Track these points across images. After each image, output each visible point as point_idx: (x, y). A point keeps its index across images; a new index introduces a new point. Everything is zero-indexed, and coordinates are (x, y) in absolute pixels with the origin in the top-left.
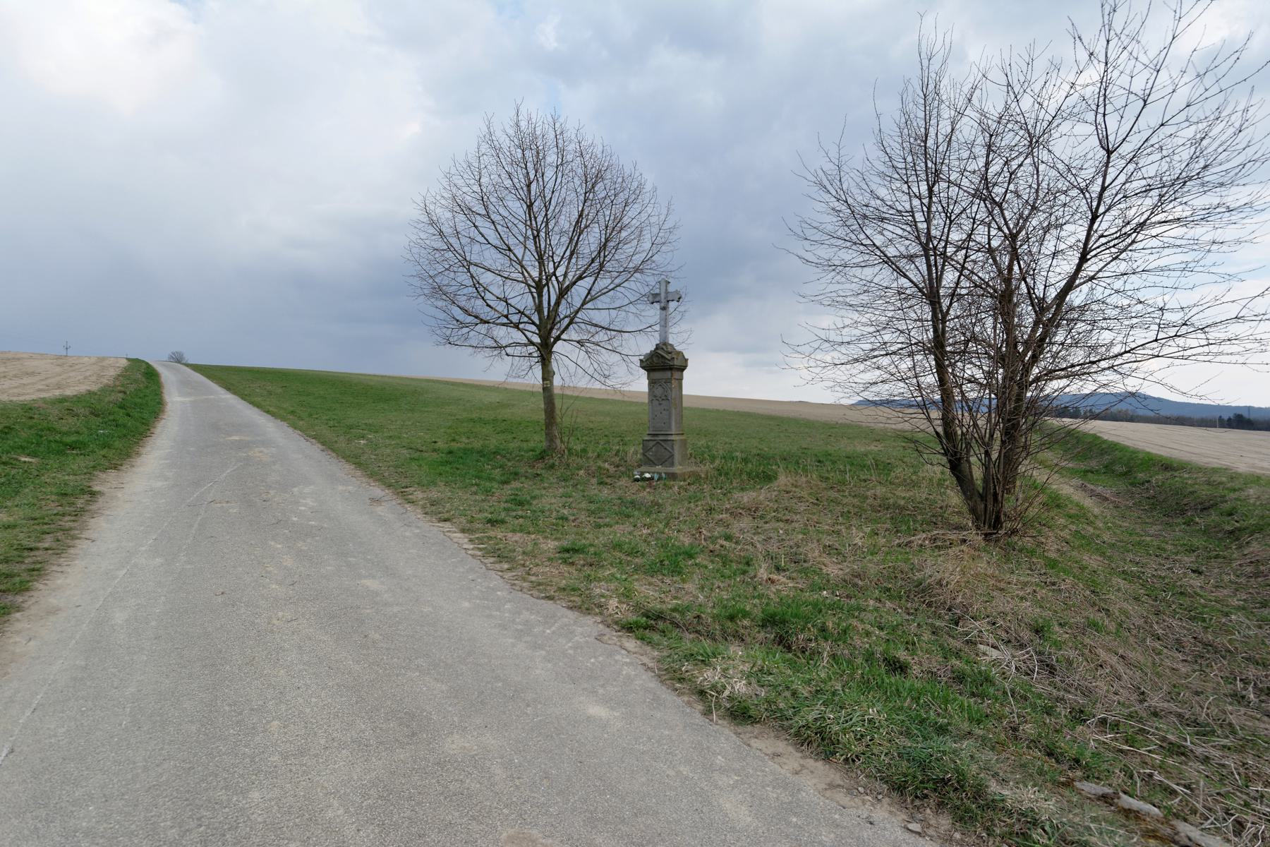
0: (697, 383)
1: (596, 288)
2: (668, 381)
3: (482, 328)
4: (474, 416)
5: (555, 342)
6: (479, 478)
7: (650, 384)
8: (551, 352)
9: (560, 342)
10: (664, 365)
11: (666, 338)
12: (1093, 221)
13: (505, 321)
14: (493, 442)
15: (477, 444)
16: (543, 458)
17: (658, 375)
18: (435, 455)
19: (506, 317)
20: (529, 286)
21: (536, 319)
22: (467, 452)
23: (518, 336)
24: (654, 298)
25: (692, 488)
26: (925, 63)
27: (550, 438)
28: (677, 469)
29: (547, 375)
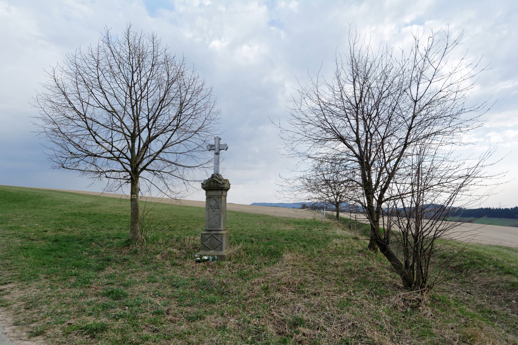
0: (236, 197)
1: (173, 139)
2: (220, 197)
3: (90, 159)
4: (76, 211)
5: (142, 170)
6: (77, 266)
7: (207, 198)
8: (138, 177)
9: (144, 171)
10: (216, 187)
11: (218, 171)
12: (409, 130)
13: (109, 155)
14: (89, 230)
15: (77, 233)
16: (128, 245)
17: (212, 193)
18: (43, 243)
19: (111, 152)
20: (125, 134)
21: (129, 155)
22: (69, 239)
23: (117, 166)
24: (211, 148)
25: (236, 266)
26: (352, 46)
27: (134, 231)
28: (225, 252)
29: (135, 190)
